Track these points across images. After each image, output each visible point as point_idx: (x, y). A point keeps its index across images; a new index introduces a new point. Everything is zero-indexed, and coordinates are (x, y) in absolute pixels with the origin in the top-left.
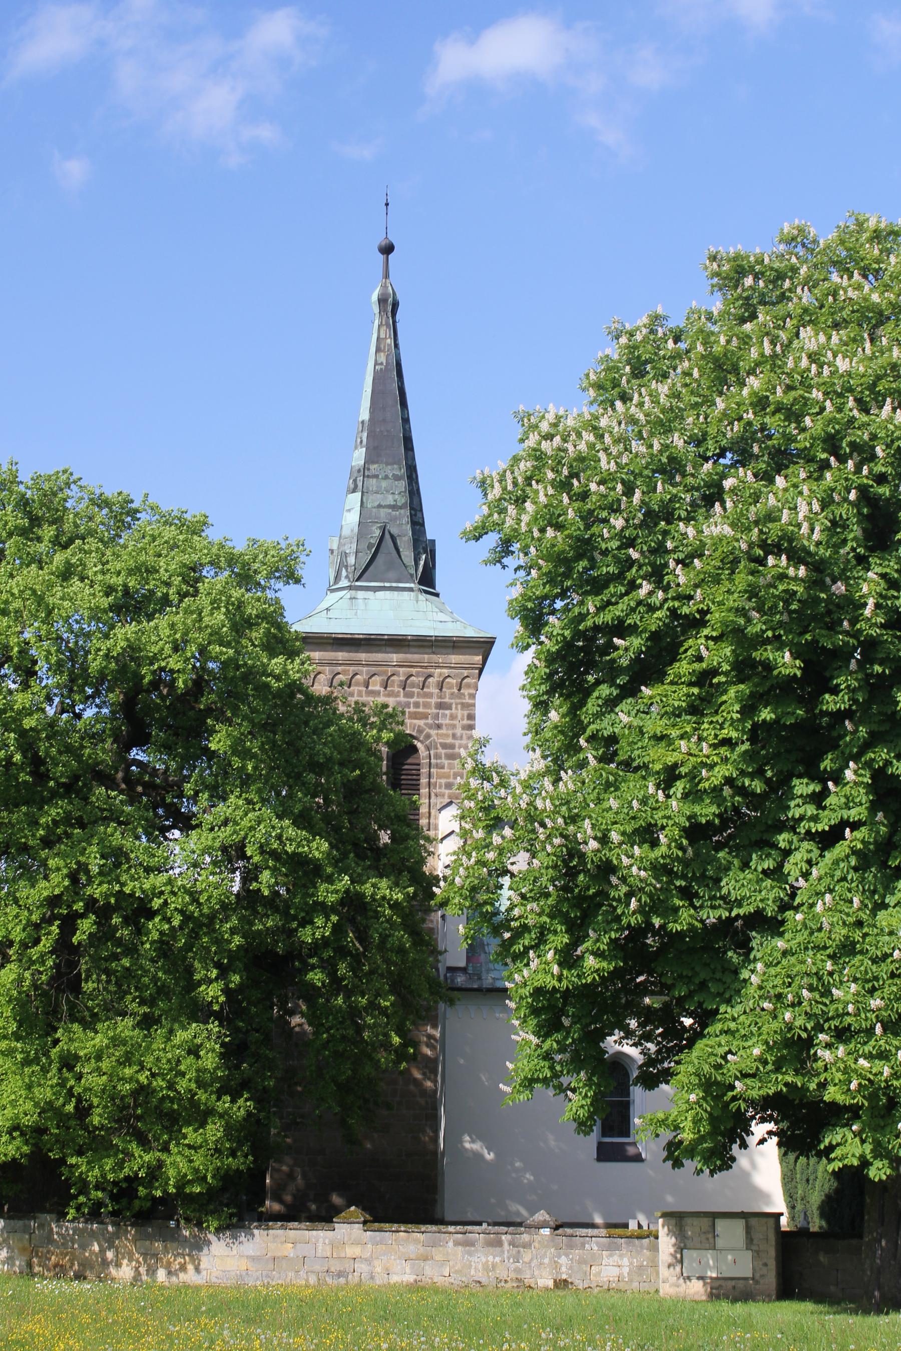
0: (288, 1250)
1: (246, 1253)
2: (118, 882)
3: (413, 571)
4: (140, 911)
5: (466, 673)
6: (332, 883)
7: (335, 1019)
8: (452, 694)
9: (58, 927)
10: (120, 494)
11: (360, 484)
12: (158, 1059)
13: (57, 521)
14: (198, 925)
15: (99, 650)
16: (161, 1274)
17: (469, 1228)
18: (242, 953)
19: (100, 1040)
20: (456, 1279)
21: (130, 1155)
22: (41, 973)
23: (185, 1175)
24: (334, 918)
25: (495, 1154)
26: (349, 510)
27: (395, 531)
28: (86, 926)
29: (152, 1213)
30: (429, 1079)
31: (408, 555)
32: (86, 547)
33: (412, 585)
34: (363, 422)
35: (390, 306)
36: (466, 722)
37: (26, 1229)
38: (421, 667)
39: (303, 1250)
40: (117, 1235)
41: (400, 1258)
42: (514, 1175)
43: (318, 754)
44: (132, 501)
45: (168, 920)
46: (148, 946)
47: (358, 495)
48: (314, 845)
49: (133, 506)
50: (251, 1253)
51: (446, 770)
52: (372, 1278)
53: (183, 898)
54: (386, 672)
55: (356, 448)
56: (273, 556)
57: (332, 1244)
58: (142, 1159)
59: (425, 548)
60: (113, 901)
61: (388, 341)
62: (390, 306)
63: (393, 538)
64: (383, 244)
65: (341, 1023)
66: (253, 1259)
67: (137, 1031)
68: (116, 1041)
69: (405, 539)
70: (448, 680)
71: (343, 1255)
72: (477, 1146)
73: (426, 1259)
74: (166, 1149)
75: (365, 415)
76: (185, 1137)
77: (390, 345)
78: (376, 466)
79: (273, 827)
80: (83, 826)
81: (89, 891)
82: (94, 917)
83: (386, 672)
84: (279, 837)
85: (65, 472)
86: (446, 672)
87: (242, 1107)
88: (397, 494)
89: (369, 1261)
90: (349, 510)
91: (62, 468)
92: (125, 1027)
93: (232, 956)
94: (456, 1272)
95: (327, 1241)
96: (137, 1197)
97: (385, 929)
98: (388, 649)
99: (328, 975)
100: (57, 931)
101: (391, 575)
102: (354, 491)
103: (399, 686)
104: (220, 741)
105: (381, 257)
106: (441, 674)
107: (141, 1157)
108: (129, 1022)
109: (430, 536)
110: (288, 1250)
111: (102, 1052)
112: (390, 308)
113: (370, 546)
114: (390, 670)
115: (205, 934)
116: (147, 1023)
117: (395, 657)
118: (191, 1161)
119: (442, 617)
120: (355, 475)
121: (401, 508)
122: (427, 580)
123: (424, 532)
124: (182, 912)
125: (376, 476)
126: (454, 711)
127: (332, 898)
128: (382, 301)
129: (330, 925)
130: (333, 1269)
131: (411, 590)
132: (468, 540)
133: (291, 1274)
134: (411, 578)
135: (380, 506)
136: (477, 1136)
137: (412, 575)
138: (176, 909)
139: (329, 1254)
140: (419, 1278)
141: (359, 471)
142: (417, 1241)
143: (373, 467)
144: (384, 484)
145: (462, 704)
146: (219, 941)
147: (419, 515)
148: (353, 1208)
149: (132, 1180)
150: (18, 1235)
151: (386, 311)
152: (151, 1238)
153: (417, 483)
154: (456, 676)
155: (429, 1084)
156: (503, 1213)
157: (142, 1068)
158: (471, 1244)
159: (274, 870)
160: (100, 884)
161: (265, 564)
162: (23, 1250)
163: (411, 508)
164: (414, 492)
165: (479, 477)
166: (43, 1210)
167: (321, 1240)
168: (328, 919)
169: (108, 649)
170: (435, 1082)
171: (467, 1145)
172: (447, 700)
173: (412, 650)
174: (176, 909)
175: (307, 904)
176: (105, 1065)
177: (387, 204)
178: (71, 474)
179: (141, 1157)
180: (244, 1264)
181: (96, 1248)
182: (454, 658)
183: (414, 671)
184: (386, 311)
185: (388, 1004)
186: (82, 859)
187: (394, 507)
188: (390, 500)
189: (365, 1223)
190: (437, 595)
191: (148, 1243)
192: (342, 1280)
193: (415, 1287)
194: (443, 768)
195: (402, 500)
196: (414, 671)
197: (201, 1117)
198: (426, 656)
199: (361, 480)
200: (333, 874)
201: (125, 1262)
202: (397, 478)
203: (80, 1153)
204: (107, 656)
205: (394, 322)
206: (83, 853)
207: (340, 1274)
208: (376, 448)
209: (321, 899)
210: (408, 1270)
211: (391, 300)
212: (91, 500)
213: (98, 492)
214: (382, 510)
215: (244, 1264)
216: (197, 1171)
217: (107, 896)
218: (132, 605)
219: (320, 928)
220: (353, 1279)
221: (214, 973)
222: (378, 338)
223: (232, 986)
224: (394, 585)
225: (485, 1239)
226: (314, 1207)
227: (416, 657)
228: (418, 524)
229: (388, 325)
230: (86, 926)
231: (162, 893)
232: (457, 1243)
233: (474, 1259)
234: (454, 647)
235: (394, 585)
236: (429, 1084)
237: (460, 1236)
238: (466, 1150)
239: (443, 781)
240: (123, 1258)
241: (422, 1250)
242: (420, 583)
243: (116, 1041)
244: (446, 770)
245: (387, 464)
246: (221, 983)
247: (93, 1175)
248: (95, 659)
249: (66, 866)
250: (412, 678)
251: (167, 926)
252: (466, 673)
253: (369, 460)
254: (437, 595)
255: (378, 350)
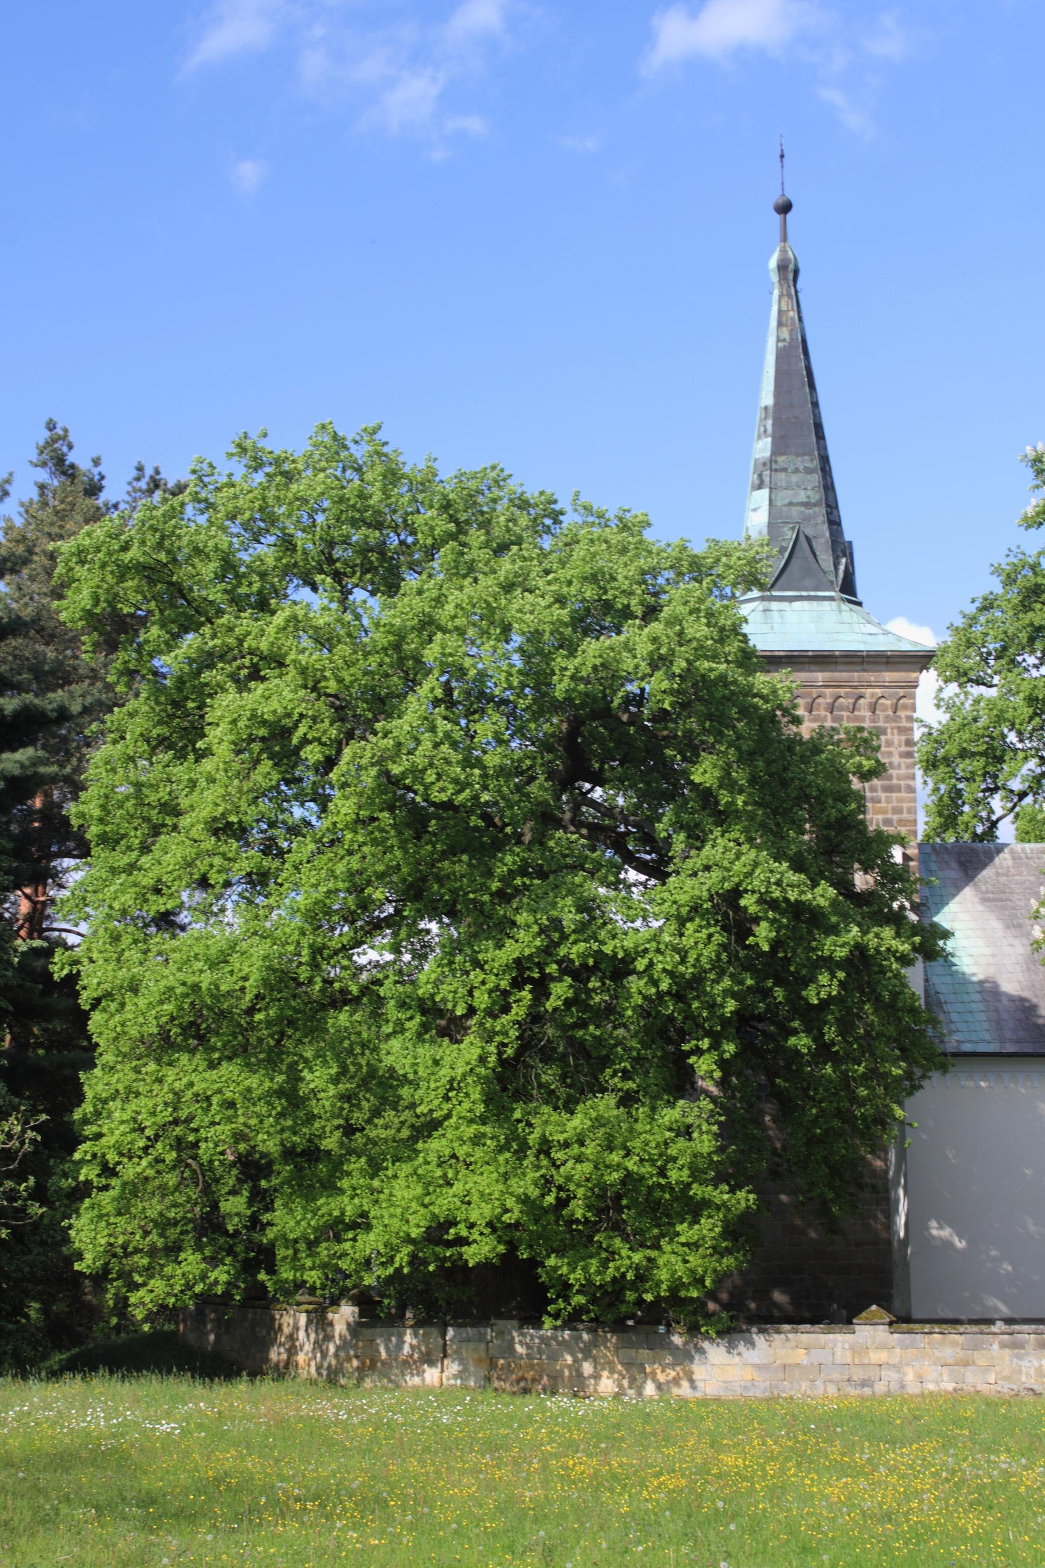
0: (800, 1356)
1: (751, 1361)
2: (596, 940)
3: (832, 578)
4: (619, 969)
5: (901, 692)
6: (837, 934)
7: (826, 1090)
8: (887, 717)
9: (530, 992)
10: (542, 493)
11: (767, 479)
12: (646, 1143)
13: (486, 525)
14: (686, 988)
15: (566, 669)
16: (650, 1389)
17: (1017, 1327)
18: (735, 1018)
19: (577, 1122)
20: (1005, 1388)
21: (613, 1254)
22: (505, 1045)
23: (681, 1278)
24: (841, 975)
25: (968, 1242)
26: (755, 510)
27: (809, 532)
28: (561, 990)
29: (640, 1319)
30: (879, 1158)
31: (826, 558)
32: (526, 554)
33: (833, 594)
34: (766, 408)
35: (790, 272)
36: (903, 749)
37: (482, 1338)
38: (850, 687)
39: (818, 1356)
40: (594, 1344)
41: (935, 1364)
42: (989, 1265)
43: (809, 785)
44: (555, 502)
45: (655, 983)
46: (629, 1013)
47: (765, 493)
48: (818, 890)
49: (557, 507)
50: (757, 1361)
51: (883, 804)
52: (903, 1387)
53: (672, 957)
54: (810, 694)
55: (759, 438)
56: (739, 559)
57: (852, 1349)
58: (629, 1258)
59: (842, 549)
60: (591, 962)
61: (791, 314)
62: (790, 272)
63: (807, 538)
64: (781, 201)
65: (834, 1094)
66: (759, 1367)
67: (622, 1109)
68: (599, 1122)
69: (822, 540)
70: (882, 701)
71: (866, 1361)
72: (946, 1233)
73: (966, 1364)
74: (657, 1247)
75: (767, 398)
76: (678, 1234)
77: (792, 319)
78: (783, 458)
79: (771, 871)
80: (543, 875)
81: (562, 951)
82: (569, 980)
83: (810, 694)
84: (778, 883)
85: (494, 468)
86: (879, 691)
87: (745, 1199)
88: (810, 490)
89: (897, 1367)
90: (755, 510)
91: (490, 464)
92: (606, 1105)
93: (725, 1022)
94: (1005, 1378)
95: (846, 1346)
96: (623, 1302)
97: (894, 986)
98: (812, 667)
99: (814, 1040)
100: (530, 996)
101: (807, 582)
102: (760, 487)
103: (826, 710)
104: (705, 772)
105: (777, 218)
106: (873, 695)
107: (629, 1258)
108: (611, 1099)
109: (848, 537)
110: (800, 1356)
111: (584, 1137)
112: (791, 276)
113: (782, 550)
114: (815, 692)
115: (694, 998)
116: (627, 1100)
117: (820, 677)
118: (686, 1262)
119: (871, 629)
120: (761, 468)
121: (815, 505)
122: (848, 587)
123: (841, 533)
124: (671, 974)
125: (785, 470)
126: (889, 736)
127: (841, 953)
128: (782, 267)
129: (835, 982)
130: (855, 1378)
131: (831, 599)
132: (1029, 527)
133: (804, 1385)
134: (830, 586)
135: (791, 504)
136: (944, 1221)
137: (832, 582)
138: (664, 970)
139: (849, 1360)
140: (959, 1386)
141: (764, 464)
142: (954, 1344)
143: (781, 459)
144: (794, 478)
145: (899, 728)
146: (712, 1006)
147: (835, 512)
148: (874, 1307)
149: (619, 1281)
150: (472, 1345)
151: (786, 279)
152: (636, 1346)
153: (831, 476)
154: (891, 696)
155: (879, 1163)
156: (978, 1309)
157: (628, 1153)
158: (1020, 1346)
159: (773, 922)
160: (575, 942)
161: (731, 568)
162: (479, 1361)
163: (828, 506)
164: (829, 487)
165: (1031, 455)
166: (500, 1316)
167: (839, 1345)
168: (833, 976)
169: (576, 669)
170: (886, 1160)
171: (935, 1232)
172: (881, 724)
173: (840, 667)
174: (664, 970)
175: (809, 959)
176: (590, 1149)
177: (782, 156)
178: (502, 470)
179: (629, 1258)
180: (749, 1374)
181: (569, 1359)
182: (888, 676)
183: (842, 691)
184: (786, 279)
185: (900, 1072)
186: (554, 913)
187: (807, 505)
188: (802, 496)
189: (891, 1324)
190: (860, 604)
191: (633, 1352)
192: (867, 1391)
193: (956, 1398)
194: (879, 802)
195: (816, 496)
196: (842, 691)
197: (695, 1209)
198: (856, 674)
199: (767, 474)
200: (838, 924)
201: (605, 1373)
202: (809, 471)
203: (560, 1252)
204: (573, 678)
205: (796, 292)
206: (554, 905)
207: (865, 1383)
208: (783, 437)
209: (827, 953)
210: (945, 1378)
211: (791, 266)
212: (511, 500)
213: (519, 491)
214: (793, 508)
215: (749, 1374)
216: (692, 1271)
217: (583, 956)
218: (599, 615)
219: (825, 986)
220: (880, 1388)
221: (705, 1044)
222: (780, 311)
223: (727, 1056)
224: (812, 593)
225: (1037, 1340)
226: (753, 1306)
227: (845, 675)
228: (834, 523)
229: (789, 295)
230: (561, 990)
231: (646, 951)
232: (1003, 1346)
233: (1025, 1363)
234: (887, 663)
235: (812, 593)
236: (879, 1163)
237: (1006, 1337)
238: (934, 1237)
239: (880, 817)
240: (604, 1369)
241: (961, 1354)
242: (842, 591)
243: (599, 1122)
244: (883, 804)
245: (797, 455)
246: (714, 1055)
247: (576, 1277)
248: (561, 680)
249: (536, 922)
250: (841, 700)
251: (653, 990)
252: (901, 692)
253: (776, 451)
254: (860, 604)
255: (780, 324)
